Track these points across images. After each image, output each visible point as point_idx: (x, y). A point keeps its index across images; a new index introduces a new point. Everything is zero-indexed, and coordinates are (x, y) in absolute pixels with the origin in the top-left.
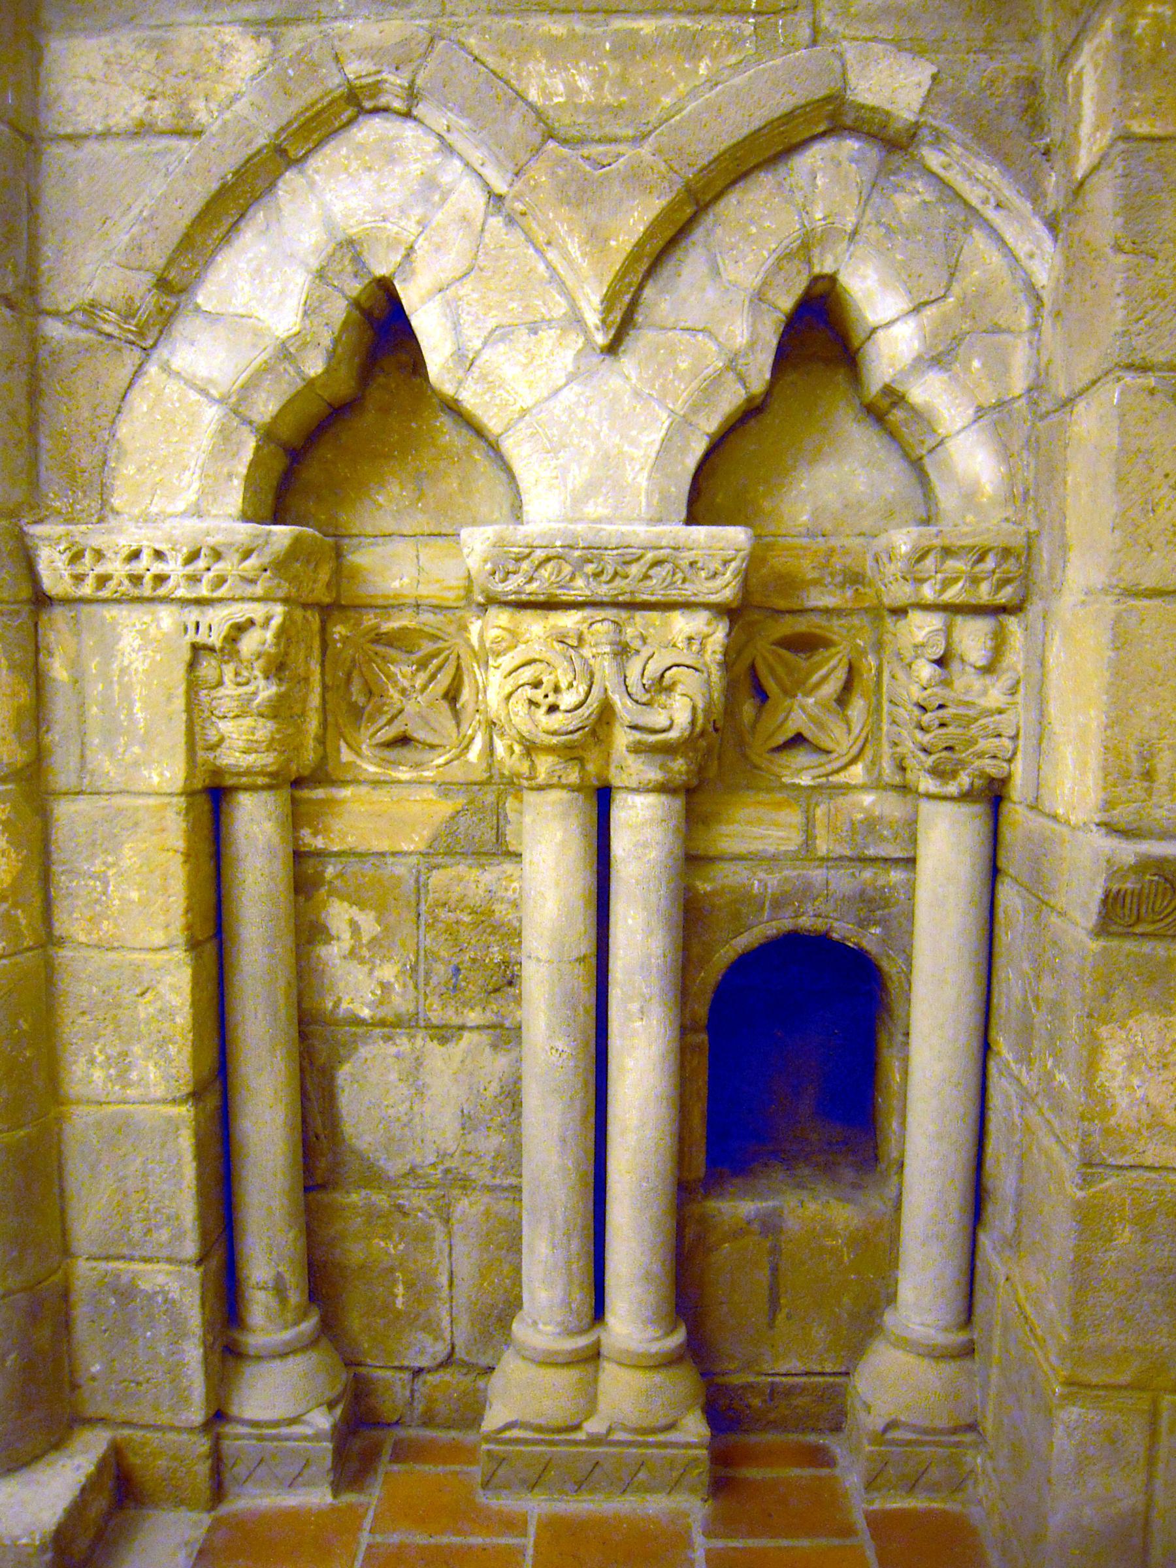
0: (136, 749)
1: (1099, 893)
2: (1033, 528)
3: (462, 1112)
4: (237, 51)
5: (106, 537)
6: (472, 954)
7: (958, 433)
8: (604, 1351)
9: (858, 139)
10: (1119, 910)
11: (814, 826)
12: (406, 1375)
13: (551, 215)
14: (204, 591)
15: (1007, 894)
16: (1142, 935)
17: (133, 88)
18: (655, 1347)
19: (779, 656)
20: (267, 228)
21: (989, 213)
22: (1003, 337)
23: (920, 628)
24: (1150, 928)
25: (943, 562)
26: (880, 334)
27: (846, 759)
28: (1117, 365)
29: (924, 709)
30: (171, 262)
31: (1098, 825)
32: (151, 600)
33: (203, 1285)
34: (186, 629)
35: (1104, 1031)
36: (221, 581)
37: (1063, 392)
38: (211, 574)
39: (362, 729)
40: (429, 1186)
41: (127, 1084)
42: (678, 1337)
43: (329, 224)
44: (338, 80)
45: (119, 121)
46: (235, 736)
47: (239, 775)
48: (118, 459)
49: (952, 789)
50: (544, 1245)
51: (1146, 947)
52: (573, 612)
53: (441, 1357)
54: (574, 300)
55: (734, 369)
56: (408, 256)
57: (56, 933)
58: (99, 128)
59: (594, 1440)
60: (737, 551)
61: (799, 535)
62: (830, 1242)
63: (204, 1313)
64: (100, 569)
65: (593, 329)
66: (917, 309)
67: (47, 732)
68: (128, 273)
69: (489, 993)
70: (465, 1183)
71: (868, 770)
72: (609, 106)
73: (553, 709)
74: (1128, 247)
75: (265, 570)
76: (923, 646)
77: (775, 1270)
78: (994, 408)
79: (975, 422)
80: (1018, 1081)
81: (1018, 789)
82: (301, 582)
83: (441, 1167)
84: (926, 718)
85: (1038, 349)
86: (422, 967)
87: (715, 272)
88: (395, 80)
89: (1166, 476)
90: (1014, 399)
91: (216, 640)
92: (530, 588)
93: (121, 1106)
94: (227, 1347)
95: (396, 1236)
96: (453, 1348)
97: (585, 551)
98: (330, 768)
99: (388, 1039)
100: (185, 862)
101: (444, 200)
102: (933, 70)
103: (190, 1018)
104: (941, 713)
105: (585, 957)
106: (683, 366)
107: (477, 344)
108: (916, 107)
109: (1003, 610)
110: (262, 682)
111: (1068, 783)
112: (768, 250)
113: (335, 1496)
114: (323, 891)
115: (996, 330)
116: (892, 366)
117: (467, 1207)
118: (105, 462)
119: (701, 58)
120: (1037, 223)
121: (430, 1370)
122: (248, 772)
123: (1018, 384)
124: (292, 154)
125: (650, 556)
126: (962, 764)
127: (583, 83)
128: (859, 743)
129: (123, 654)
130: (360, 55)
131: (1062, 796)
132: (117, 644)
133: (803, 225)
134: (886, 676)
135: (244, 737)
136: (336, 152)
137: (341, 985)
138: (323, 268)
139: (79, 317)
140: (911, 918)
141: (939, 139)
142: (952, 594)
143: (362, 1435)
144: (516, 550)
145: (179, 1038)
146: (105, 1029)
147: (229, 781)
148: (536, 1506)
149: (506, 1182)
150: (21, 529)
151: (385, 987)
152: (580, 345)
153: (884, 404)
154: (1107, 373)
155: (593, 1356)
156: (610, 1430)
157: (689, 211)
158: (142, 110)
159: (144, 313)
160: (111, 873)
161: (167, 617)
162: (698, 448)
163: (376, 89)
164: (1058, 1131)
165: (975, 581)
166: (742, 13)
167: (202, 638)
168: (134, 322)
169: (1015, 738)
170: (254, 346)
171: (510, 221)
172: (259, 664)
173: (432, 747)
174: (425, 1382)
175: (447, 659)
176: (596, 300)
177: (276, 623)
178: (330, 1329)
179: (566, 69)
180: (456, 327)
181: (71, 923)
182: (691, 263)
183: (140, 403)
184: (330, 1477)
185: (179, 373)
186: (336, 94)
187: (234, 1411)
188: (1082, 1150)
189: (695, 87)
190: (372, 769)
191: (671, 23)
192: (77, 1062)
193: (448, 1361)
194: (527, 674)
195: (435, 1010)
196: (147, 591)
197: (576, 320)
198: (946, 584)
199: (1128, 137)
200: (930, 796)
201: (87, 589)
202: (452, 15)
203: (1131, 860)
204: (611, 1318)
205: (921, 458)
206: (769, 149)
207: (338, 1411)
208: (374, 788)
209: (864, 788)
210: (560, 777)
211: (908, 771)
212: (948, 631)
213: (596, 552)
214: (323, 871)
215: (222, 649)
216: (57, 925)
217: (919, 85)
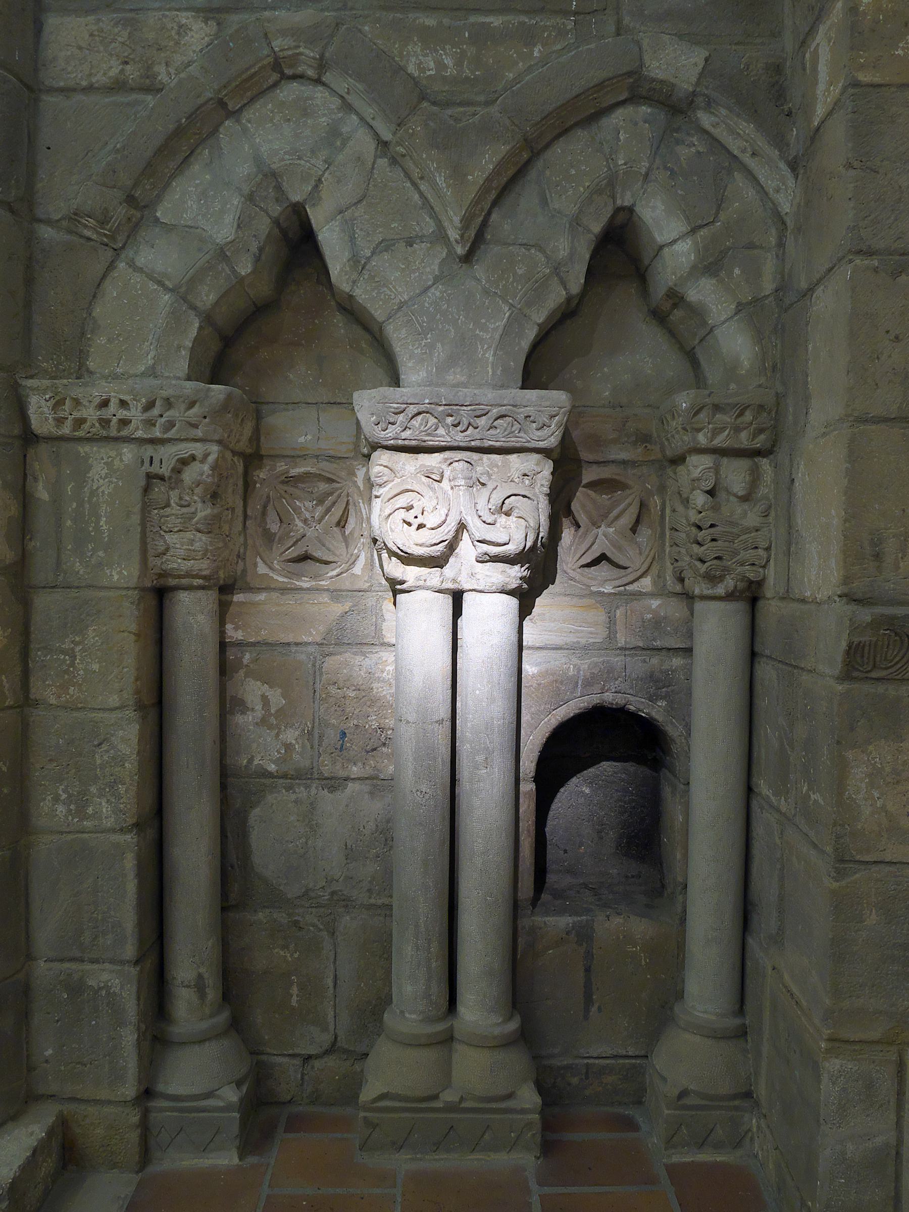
0: (101, 554)
1: (844, 645)
2: (780, 389)
3: (346, 845)
4: (191, 30)
5: (81, 390)
6: (356, 722)
7: (724, 323)
8: (457, 1035)
9: (650, 106)
10: (859, 659)
11: (615, 624)
12: (297, 1062)
13: (424, 156)
14: (157, 433)
15: (766, 672)
16: (878, 679)
17: (111, 55)
18: (497, 1031)
19: (589, 495)
20: (211, 162)
21: (747, 159)
22: (756, 251)
23: (696, 467)
24: (883, 674)
25: (714, 415)
26: (666, 250)
27: (639, 573)
28: (850, 251)
29: (699, 528)
30: (135, 185)
31: (840, 596)
32: (116, 439)
33: (139, 982)
34: (143, 462)
35: (850, 755)
36: (171, 424)
37: (804, 285)
38: (163, 420)
39: (274, 548)
40: (319, 906)
41: (86, 817)
42: (513, 1026)
43: (258, 160)
44: (266, 52)
45: (99, 79)
46: (177, 546)
47: (179, 577)
48: (92, 332)
49: (720, 590)
50: (410, 948)
51: (881, 688)
52: (436, 454)
53: (326, 1045)
54: (440, 221)
55: (557, 275)
56: (316, 186)
57: (32, 697)
58: (84, 83)
59: (451, 1108)
60: (561, 408)
61: (604, 406)
62: (630, 948)
63: (138, 1005)
64: (77, 415)
65: (454, 243)
66: (694, 231)
67: (31, 539)
68: (104, 189)
69: (368, 752)
70: (347, 903)
71: (654, 583)
72: (467, 78)
73: (421, 526)
74: (856, 164)
75: (205, 417)
76: (698, 479)
77: (588, 970)
78: (750, 303)
79: (736, 314)
80: (778, 810)
81: (770, 590)
82: (231, 431)
83: (329, 891)
84: (701, 535)
85: (783, 260)
86: (316, 731)
87: (544, 202)
88: (309, 53)
89: (888, 332)
90: (766, 297)
91: (165, 471)
92: (405, 435)
93: (80, 835)
94: (157, 1036)
95: (292, 946)
96: (336, 1038)
97: (446, 407)
98: (248, 579)
99: (289, 788)
100: (136, 641)
101: (344, 144)
102: (707, 54)
103: (136, 764)
104: (712, 530)
105: (443, 720)
106: (520, 272)
107: (368, 253)
108: (694, 80)
109: (758, 453)
110: (200, 505)
111: (818, 570)
112: (584, 187)
113: (240, 1160)
114: (242, 673)
115: (751, 246)
116: (674, 274)
117: (348, 923)
118: (83, 334)
119: (535, 45)
120: (782, 165)
121: (317, 1057)
122: (188, 575)
123: (768, 286)
124: (230, 107)
125: (495, 411)
126: (727, 570)
127: (449, 61)
128: (649, 560)
129: (93, 480)
130: (283, 33)
131: (810, 581)
132: (88, 472)
133: (610, 169)
134: (668, 511)
135: (185, 547)
136: (264, 107)
137: (254, 745)
138: (253, 192)
139: (65, 223)
140: (689, 693)
141: (709, 104)
142: (720, 441)
143: (262, 1114)
144: (395, 405)
145: (128, 780)
146: (67, 773)
147: (172, 582)
148: (403, 1163)
149: (380, 902)
150: (16, 381)
151: (288, 747)
152: (444, 255)
153: (667, 306)
154: (840, 260)
155: (447, 1040)
156: (462, 1099)
157: (526, 156)
158: (117, 71)
159: (117, 219)
160: (78, 649)
161: (128, 453)
162: (531, 334)
163: (294, 59)
164: (814, 839)
165: (737, 430)
166: (566, 13)
167: (155, 469)
168: (108, 227)
169: (768, 549)
170: (200, 250)
171: (394, 161)
172: (198, 491)
173: (327, 563)
174: (313, 1067)
175: (339, 496)
176: (457, 220)
177: (211, 459)
178: (237, 1025)
179: (436, 51)
180: (352, 239)
181: (46, 690)
182: (527, 198)
183: (111, 290)
184: (237, 1142)
185: (141, 268)
186: (265, 62)
187: (161, 1087)
188: (836, 850)
189: (531, 66)
190: (281, 579)
191: (515, 19)
192: (44, 799)
193: (332, 1049)
194: (402, 501)
195: (326, 765)
196: (113, 433)
197: (441, 236)
198: (715, 432)
199: (856, 84)
200: (704, 598)
201: (66, 430)
202: (352, 9)
203: (869, 619)
204: (461, 1009)
205: (694, 348)
206: (582, 113)
207: (244, 1089)
208: (282, 594)
209: (652, 595)
210: (425, 581)
211: (686, 581)
212: (717, 469)
213: (455, 407)
214: (242, 658)
215: (170, 478)
216: (33, 690)
217: (696, 64)
